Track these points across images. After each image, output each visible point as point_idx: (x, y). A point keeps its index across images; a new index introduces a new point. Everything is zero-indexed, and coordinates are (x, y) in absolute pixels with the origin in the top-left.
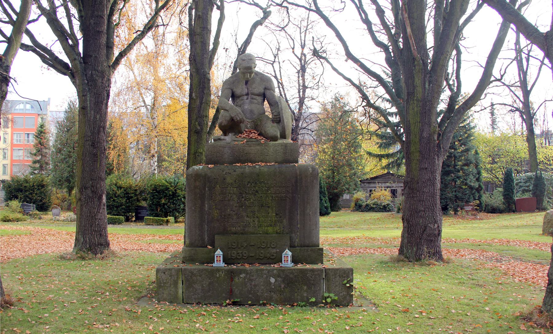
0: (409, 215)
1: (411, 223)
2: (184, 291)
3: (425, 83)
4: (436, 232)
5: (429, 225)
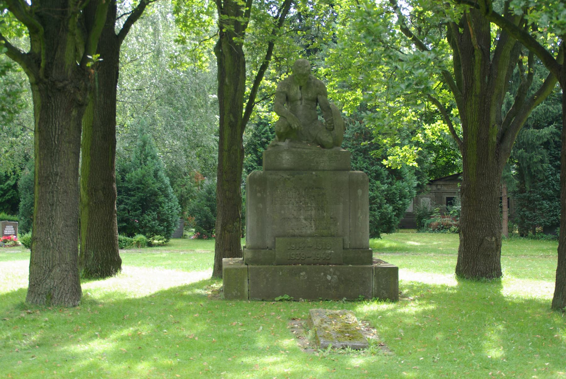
0: (465, 226)
1: (467, 236)
2: (250, 289)
3: (484, 77)
4: (494, 246)
5: (486, 238)
